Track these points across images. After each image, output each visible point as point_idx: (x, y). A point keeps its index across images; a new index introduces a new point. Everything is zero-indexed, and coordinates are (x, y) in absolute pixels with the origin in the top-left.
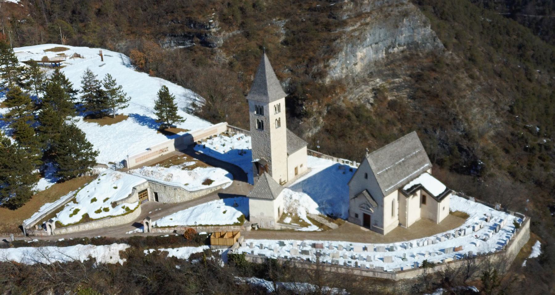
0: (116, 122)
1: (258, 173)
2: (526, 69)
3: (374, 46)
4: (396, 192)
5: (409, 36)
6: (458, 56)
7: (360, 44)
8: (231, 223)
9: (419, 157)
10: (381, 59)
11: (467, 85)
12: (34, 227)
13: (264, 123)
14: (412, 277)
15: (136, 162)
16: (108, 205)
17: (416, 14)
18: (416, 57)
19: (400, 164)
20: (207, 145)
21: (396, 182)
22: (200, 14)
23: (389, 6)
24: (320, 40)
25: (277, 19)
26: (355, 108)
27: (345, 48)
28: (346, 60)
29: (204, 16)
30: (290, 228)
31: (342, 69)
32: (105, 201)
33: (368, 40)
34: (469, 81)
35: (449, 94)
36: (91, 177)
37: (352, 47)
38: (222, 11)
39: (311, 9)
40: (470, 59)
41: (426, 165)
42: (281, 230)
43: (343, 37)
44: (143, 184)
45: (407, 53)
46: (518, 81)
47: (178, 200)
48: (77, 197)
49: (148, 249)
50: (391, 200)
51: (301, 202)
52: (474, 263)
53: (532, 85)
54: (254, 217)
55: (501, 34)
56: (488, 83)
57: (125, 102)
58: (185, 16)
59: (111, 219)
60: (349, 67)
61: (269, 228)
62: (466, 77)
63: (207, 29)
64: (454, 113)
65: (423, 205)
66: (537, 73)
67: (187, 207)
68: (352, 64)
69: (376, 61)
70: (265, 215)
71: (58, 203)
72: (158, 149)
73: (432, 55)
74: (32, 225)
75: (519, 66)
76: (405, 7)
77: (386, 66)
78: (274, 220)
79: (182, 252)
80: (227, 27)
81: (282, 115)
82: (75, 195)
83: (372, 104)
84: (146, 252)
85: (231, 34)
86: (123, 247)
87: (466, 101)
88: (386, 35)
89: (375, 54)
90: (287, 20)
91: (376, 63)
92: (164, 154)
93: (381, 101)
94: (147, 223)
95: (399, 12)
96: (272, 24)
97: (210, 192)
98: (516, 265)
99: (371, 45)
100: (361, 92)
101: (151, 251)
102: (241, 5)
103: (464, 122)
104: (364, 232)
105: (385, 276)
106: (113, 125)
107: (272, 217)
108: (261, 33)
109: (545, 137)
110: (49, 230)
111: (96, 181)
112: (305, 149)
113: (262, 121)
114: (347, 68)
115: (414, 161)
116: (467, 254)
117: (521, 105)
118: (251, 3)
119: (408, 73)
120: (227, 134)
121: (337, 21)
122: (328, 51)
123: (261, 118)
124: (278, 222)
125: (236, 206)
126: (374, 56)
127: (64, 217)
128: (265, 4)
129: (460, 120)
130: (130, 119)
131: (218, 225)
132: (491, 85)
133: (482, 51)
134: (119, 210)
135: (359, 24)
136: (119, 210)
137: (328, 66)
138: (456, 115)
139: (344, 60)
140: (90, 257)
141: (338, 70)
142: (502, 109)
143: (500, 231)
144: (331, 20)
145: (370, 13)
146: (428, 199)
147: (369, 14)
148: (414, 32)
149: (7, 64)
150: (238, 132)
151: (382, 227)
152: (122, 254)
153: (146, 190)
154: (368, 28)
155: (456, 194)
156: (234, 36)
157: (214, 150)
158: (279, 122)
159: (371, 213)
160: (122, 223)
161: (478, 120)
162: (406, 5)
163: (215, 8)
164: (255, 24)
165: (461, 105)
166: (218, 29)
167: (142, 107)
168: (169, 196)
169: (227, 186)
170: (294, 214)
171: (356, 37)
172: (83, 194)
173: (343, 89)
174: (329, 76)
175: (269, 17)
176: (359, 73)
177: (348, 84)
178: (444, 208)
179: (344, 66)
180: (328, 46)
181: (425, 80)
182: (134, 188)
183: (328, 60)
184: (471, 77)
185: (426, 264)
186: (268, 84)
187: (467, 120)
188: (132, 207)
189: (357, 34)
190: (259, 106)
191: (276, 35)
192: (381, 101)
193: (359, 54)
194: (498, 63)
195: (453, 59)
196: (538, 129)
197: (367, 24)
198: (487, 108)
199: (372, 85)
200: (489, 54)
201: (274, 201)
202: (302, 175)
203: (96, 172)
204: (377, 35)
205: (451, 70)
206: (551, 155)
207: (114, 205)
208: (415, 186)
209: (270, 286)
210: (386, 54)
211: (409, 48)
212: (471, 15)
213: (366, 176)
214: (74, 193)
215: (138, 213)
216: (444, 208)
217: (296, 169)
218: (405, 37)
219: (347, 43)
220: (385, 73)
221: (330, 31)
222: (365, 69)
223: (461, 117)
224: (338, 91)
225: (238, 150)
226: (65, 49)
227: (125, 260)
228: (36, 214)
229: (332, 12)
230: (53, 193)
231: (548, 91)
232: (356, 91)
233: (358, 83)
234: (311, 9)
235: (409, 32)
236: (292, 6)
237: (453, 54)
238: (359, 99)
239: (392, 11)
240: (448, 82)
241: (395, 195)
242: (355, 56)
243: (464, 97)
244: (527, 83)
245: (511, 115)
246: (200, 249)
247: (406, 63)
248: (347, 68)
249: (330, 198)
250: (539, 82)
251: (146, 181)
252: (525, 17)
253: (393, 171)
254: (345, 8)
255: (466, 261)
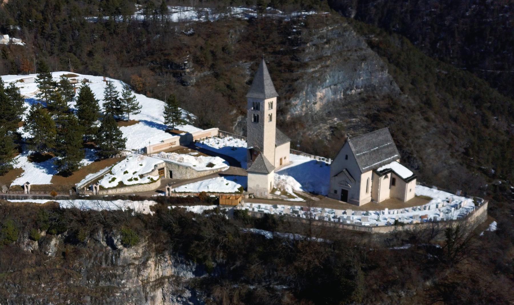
0: (130, 124)
1: (251, 159)
2: (483, 116)
3: (332, 87)
4: (371, 172)
5: (367, 79)
6: (414, 99)
7: (320, 85)
8: (233, 191)
9: (390, 148)
10: (339, 100)
11: (422, 127)
12: (84, 188)
13: (260, 117)
14: (385, 232)
15: (154, 150)
16: (137, 176)
17: (374, 58)
18: (373, 99)
19: (374, 151)
20: (205, 142)
21: (372, 164)
22: (177, 56)
23: (349, 51)
24: (282, 80)
25: (244, 61)
26: (313, 143)
27: (306, 88)
28: (306, 99)
29: (179, 58)
30: (280, 198)
31: (302, 107)
32: (134, 173)
33: (328, 81)
34: (424, 123)
35: (404, 134)
36: (120, 158)
37: (313, 87)
38: (195, 54)
39: (275, 53)
40: (425, 104)
41: (396, 156)
42: (273, 199)
43: (305, 77)
44: (162, 163)
45: (364, 95)
46: (474, 127)
47: (188, 177)
48: (112, 170)
49: (171, 206)
50: (366, 177)
51: (288, 181)
52: (438, 226)
53: (488, 131)
54: (251, 188)
55: (456, 86)
56: (443, 126)
57: (137, 109)
58: (163, 58)
59: (140, 186)
60: (309, 105)
61: (263, 197)
62: (422, 119)
63: (182, 69)
64: (409, 152)
65: (393, 187)
66: (493, 120)
67: (196, 181)
68: (312, 103)
69: (334, 102)
70: (261, 186)
71: (99, 174)
72: (169, 142)
73: (388, 97)
74: (82, 187)
75: (476, 113)
76: (364, 52)
77: (343, 106)
78: (267, 191)
79: (197, 209)
80: (199, 68)
81: (274, 112)
82: (111, 169)
83: (329, 140)
84: (169, 207)
85: (202, 74)
86: (152, 203)
87: (421, 141)
88: (344, 77)
89: (333, 95)
90: (252, 63)
91: (334, 103)
92: (173, 146)
93: (339, 139)
94: (168, 189)
95: (358, 56)
96: (238, 66)
97: (212, 172)
98: (475, 234)
99: (330, 86)
100: (319, 129)
101: (174, 207)
102: (212, 49)
103: (418, 160)
104: (342, 204)
105: (363, 230)
106: (128, 127)
107: (266, 189)
108: (229, 74)
109: (500, 179)
110: (94, 191)
111: (126, 160)
112: (288, 145)
113: (258, 116)
114: (307, 107)
115: (386, 150)
116: (433, 218)
117: (476, 148)
118: (221, 47)
119: (365, 113)
120: (219, 137)
121: (299, 63)
122: (289, 90)
123: (257, 113)
124: (270, 193)
125: (236, 181)
126: (333, 97)
127: (105, 183)
128: (233, 48)
129: (415, 158)
130: (140, 123)
131: (223, 193)
132: (446, 128)
133: (438, 97)
134: (146, 180)
135: (319, 66)
136: (146, 180)
137: (289, 104)
138: (410, 154)
139: (304, 99)
140: (129, 208)
141: (298, 108)
142: (457, 151)
143: (461, 209)
144: (294, 62)
145: (331, 56)
146: (397, 182)
147: (329, 58)
148: (371, 76)
149: (44, 79)
150: (227, 135)
151: (358, 199)
152: (152, 208)
153: (163, 168)
154: (328, 70)
155: (421, 185)
156: (205, 76)
157: (211, 146)
158: (271, 117)
159: (349, 188)
160: (148, 190)
161: (433, 159)
162: (365, 50)
163: (189, 51)
164: (224, 66)
165: (415, 145)
166: (191, 70)
167: (148, 116)
168: (181, 174)
169: (226, 169)
170: (282, 190)
171: (317, 77)
172: (117, 168)
173: (302, 126)
174: (289, 113)
175: (236, 60)
176: (317, 112)
177: (307, 121)
178: (410, 190)
179: (304, 104)
180: (290, 86)
181: (381, 120)
182: (156, 166)
183: (289, 98)
184: (427, 119)
185: (397, 223)
186: (265, 84)
187: (421, 158)
188: (155, 178)
189: (317, 75)
190: (256, 103)
191: (242, 75)
192: (339, 139)
193: (319, 94)
194: (454, 108)
195: (409, 102)
196: (493, 171)
197: (327, 66)
198: (441, 149)
199: (330, 124)
200: (444, 100)
201: (269, 175)
202: (285, 166)
203: (124, 155)
204: (336, 77)
205: (407, 112)
206: (506, 196)
207: (142, 176)
208: (386, 169)
209: (269, 235)
210: (343, 95)
211: (366, 91)
212: (427, 66)
213: (347, 158)
214: (110, 168)
215: (158, 184)
216: (410, 190)
217: (281, 159)
218: (362, 80)
219: (308, 83)
220: (343, 113)
221: (292, 72)
222: (323, 108)
223: (415, 156)
224: (298, 127)
225: (231, 147)
226: (76, 76)
227: (154, 212)
228: (83, 180)
229: (295, 54)
230: (93, 167)
231: (506, 138)
232: (314, 128)
233: (317, 121)
234: (275, 53)
235: (367, 75)
236: (257, 50)
237: (409, 97)
238: (317, 136)
239: (351, 55)
240: (404, 123)
241: (369, 174)
242: (315, 96)
243: (418, 138)
244: (483, 129)
245: (466, 156)
246: (212, 207)
247: (363, 105)
248: (307, 107)
249: (311, 181)
250: (496, 129)
251: (163, 161)
252: (482, 72)
253: (368, 155)
254: (307, 51)
255: (431, 224)
